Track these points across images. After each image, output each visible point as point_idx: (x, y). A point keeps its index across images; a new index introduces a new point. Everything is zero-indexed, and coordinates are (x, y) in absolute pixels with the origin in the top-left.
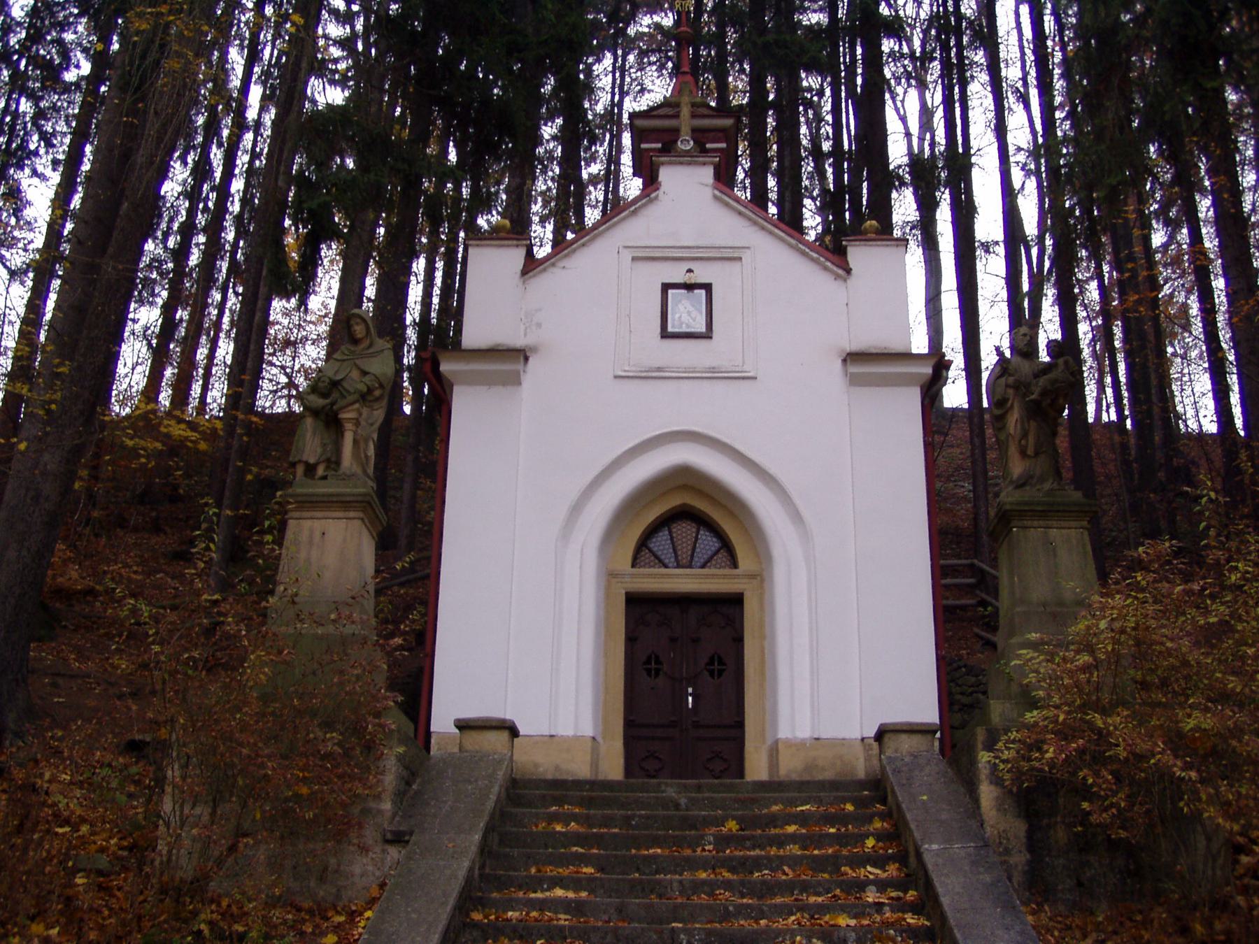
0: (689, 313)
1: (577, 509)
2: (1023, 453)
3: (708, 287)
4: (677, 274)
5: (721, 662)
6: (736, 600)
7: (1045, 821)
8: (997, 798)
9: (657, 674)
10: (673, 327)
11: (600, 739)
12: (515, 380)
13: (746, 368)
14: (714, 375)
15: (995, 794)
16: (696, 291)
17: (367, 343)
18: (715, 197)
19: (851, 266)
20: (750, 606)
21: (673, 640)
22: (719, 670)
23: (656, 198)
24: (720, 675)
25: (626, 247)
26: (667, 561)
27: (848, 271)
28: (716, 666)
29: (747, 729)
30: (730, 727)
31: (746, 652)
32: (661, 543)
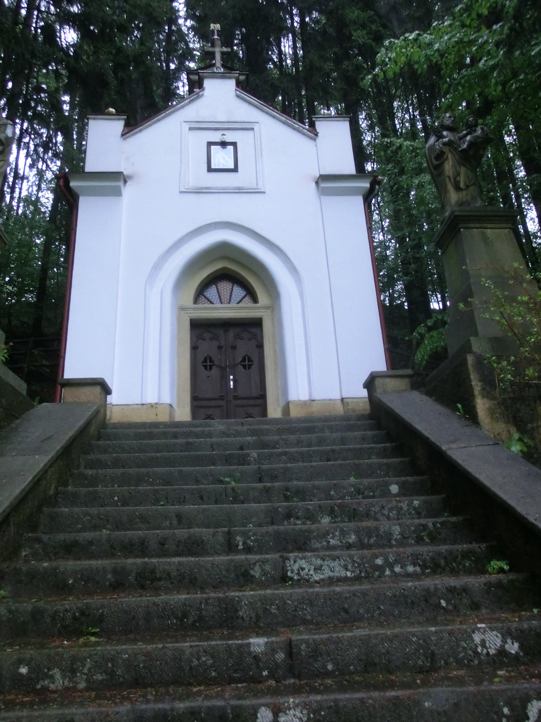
0: (224, 158)
1: (157, 266)
2: (457, 188)
3: (234, 144)
4: (216, 137)
5: (250, 360)
6: (257, 323)
7: (530, 426)
8: (490, 409)
11: (175, 406)
12: (118, 193)
14: (239, 191)
15: (487, 406)
18: (238, 96)
19: (318, 131)
20: (267, 326)
21: (220, 348)
23: (203, 95)
25: (185, 122)
27: (316, 135)
30: (256, 398)
31: (265, 353)
32: (212, 292)
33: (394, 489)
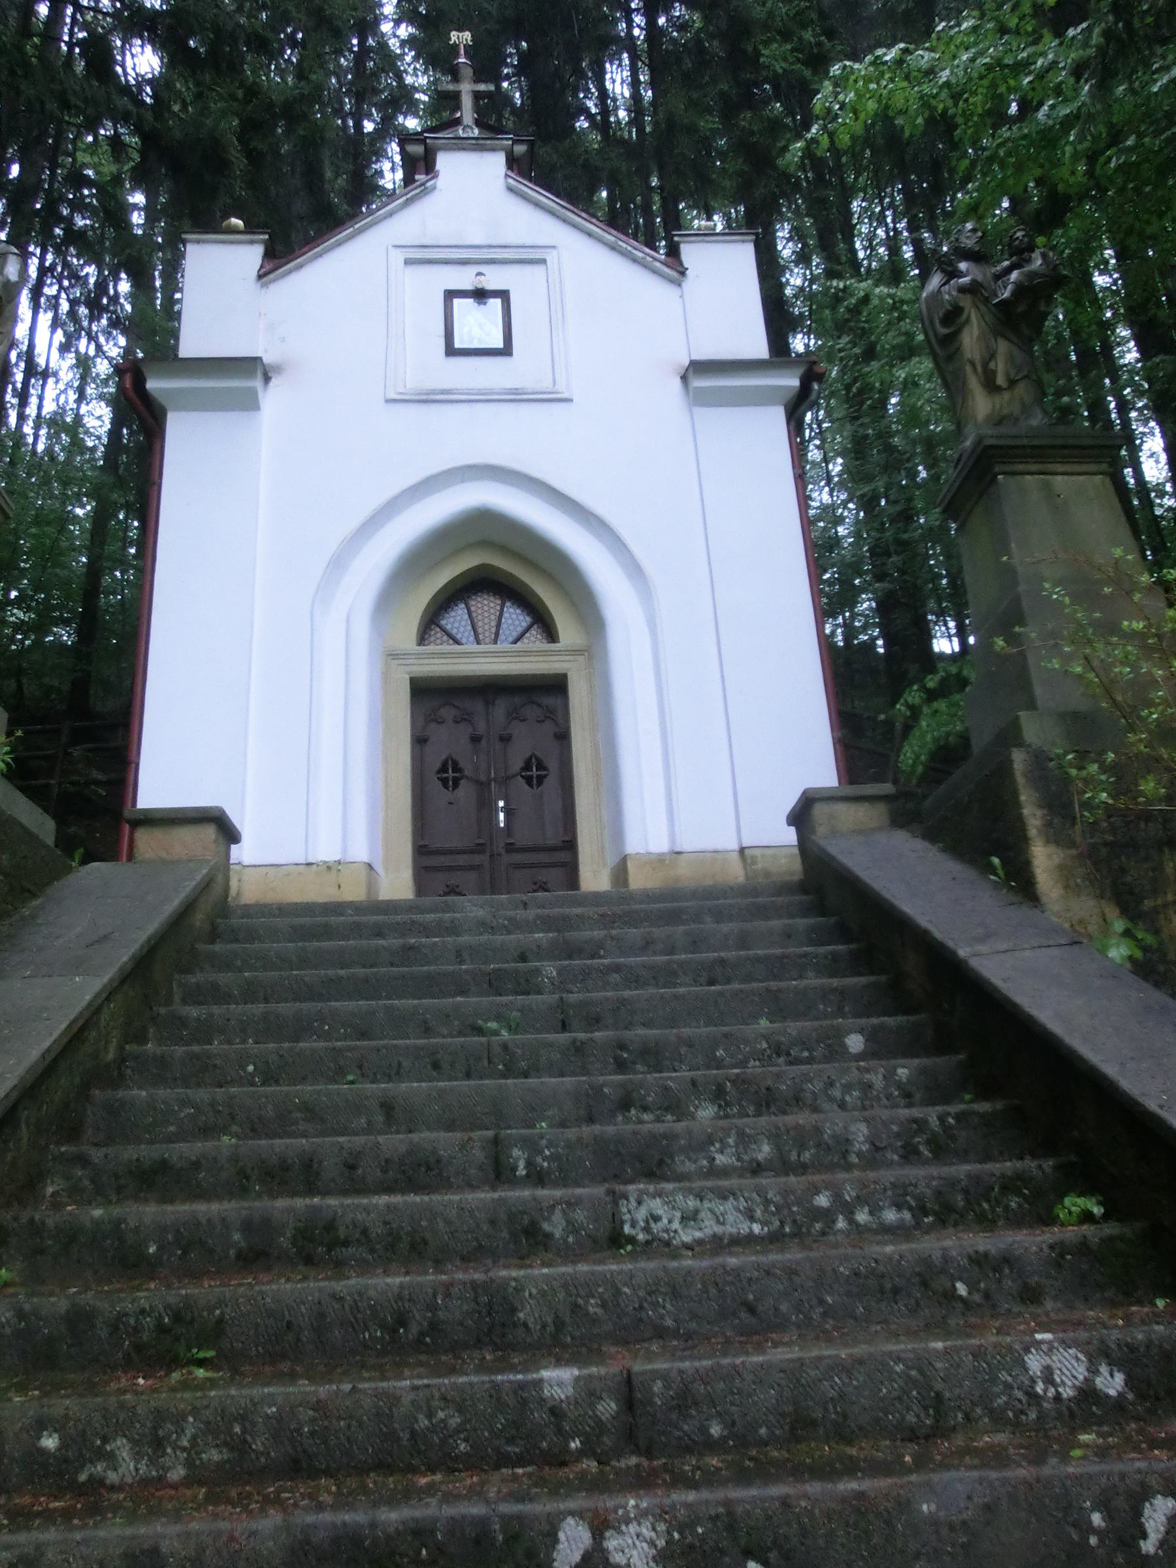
1: (339, 563)
2: (990, 386)
3: (504, 295)
4: (465, 279)
5: (541, 766)
6: (557, 686)
11: (379, 869)
12: (250, 403)
14: (516, 397)
15: (1056, 860)
18: (510, 189)
19: (686, 265)
21: (475, 739)
22: (538, 776)
23: (434, 188)
27: (683, 273)
28: (534, 772)
32: (456, 619)
33: (855, 1042)
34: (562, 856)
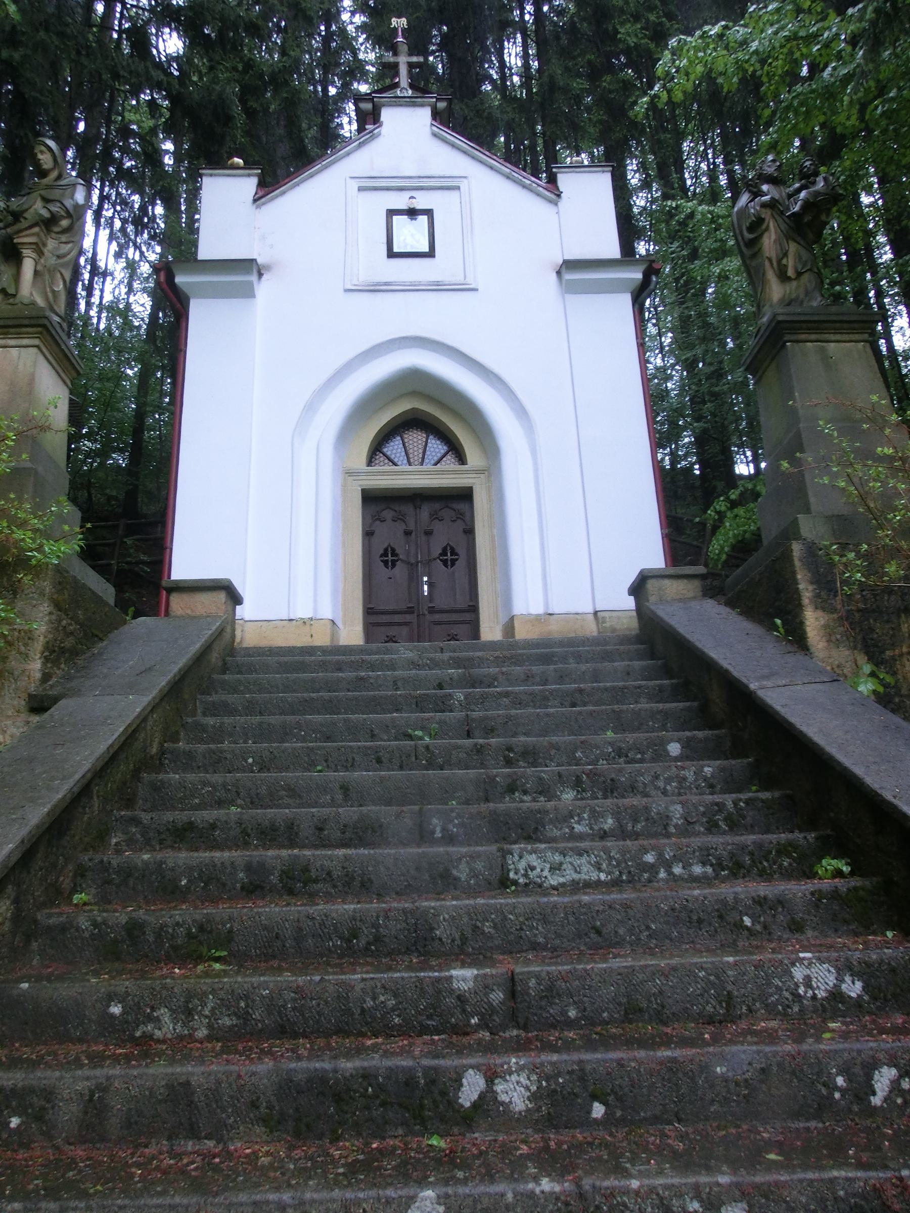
0: (412, 235)
1: (311, 407)
2: (783, 277)
3: (429, 213)
4: (401, 201)
5: (453, 553)
6: (465, 495)
8: (825, 626)
9: (394, 565)
10: (399, 247)
11: (339, 623)
12: (248, 293)
13: (468, 281)
14: (438, 287)
16: (420, 217)
17: (55, 174)
18: (435, 135)
21: (408, 533)
24: (453, 564)
25: (351, 178)
26: (396, 460)
29: (481, 611)
32: (394, 448)
33: (674, 749)
34: (468, 616)
